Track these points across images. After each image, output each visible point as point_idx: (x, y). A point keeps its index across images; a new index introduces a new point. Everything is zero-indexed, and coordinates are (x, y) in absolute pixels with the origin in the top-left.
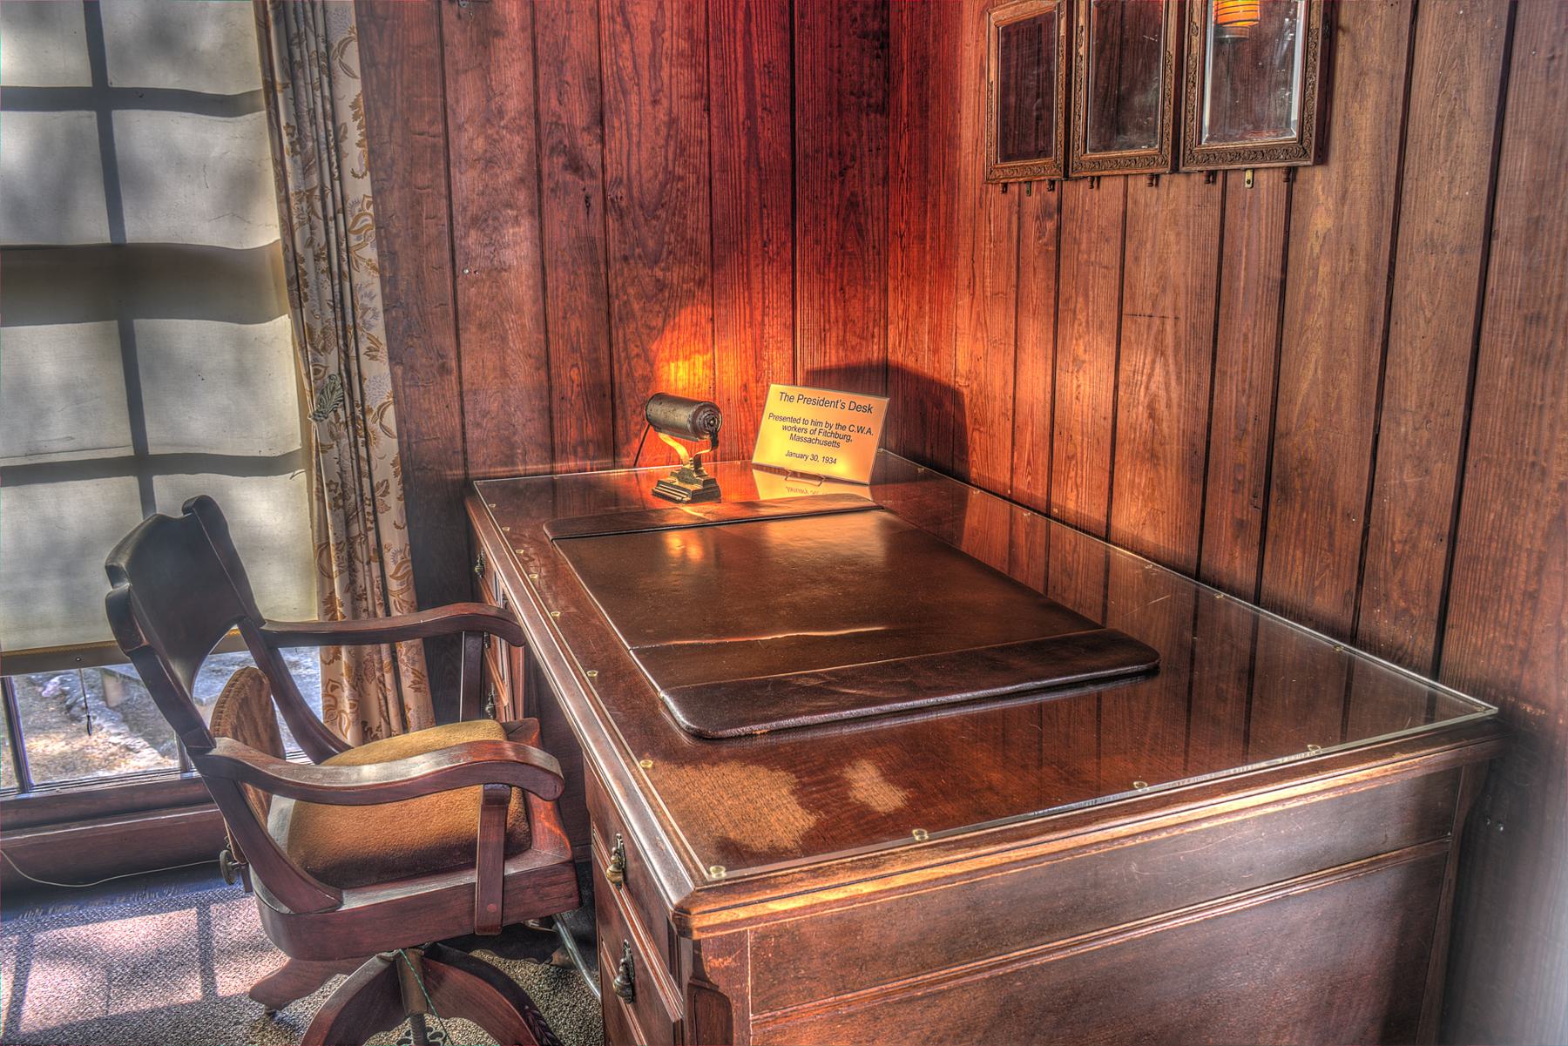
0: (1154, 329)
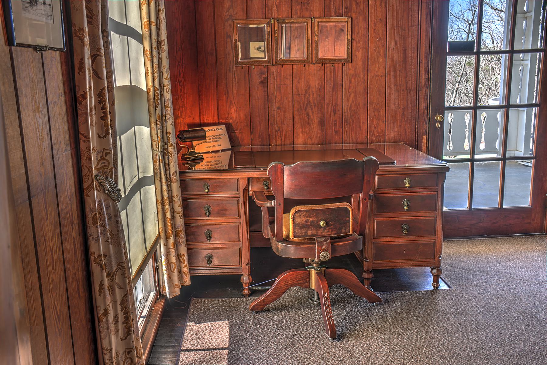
0: (307, 97)
